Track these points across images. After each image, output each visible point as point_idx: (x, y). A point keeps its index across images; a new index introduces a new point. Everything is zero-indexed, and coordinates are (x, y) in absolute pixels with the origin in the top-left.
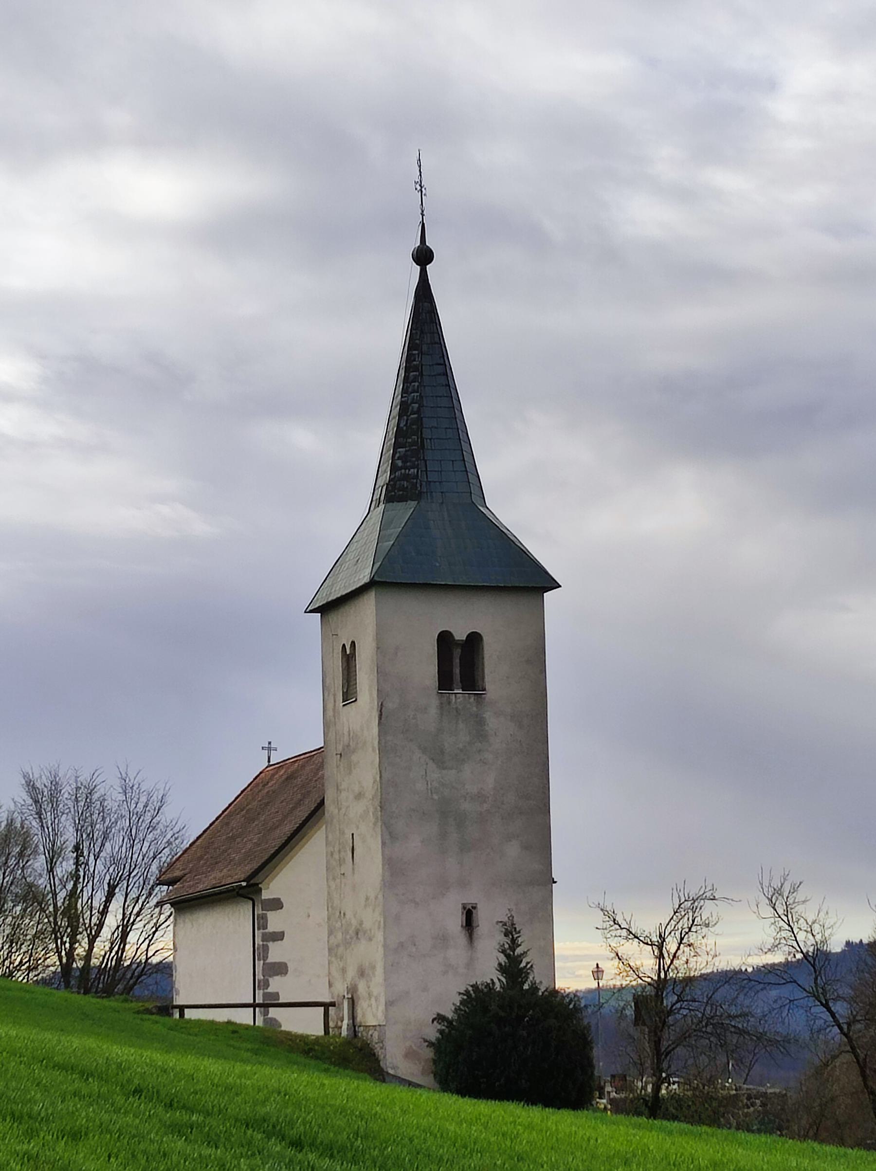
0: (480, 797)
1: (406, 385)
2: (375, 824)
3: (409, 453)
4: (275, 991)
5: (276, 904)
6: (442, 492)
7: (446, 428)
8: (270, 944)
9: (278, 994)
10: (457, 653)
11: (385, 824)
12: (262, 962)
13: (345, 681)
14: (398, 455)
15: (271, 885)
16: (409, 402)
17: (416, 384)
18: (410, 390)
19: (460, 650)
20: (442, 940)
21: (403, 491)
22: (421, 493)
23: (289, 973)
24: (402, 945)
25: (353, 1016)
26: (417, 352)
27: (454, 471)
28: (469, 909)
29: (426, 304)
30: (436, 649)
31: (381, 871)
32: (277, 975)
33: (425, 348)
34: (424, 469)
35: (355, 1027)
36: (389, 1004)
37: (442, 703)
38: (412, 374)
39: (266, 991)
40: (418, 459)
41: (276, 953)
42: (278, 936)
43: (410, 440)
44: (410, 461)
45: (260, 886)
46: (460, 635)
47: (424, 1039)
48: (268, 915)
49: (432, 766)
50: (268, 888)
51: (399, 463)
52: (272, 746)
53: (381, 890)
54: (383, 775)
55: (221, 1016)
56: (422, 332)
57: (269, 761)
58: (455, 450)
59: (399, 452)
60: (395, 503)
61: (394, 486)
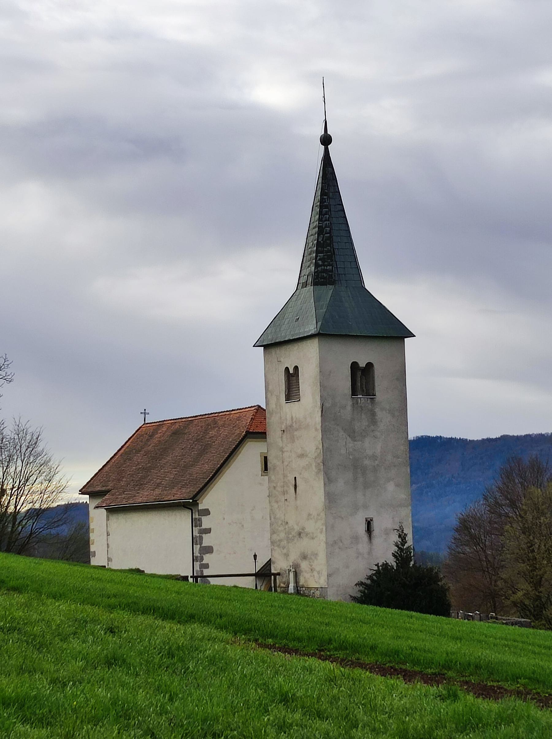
0: (374, 457)
1: (321, 216)
2: (317, 473)
3: (326, 257)
4: (207, 563)
5: (206, 512)
6: (346, 280)
7: (345, 243)
8: (204, 535)
9: (208, 564)
10: (359, 374)
11: (326, 473)
12: (199, 546)
13: (286, 388)
14: (319, 258)
15: (203, 501)
16: (324, 226)
17: (328, 216)
18: (324, 219)
19: (361, 373)
20: (355, 539)
21: (324, 279)
22: (335, 280)
23: (214, 551)
24: (335, 542)
25: (296, 582)
26: (326, 197)
27: (351, 268)
28: (369, 521)
29: (329, 169)
30: (350, 371)
31: (323, 500)
32: (207, 553)
33: (331, 194)
34: (336, 267)
35: (297, 587)
36: (329, 576)
37: (353, 404)
38: (324, 210)
39: (202, 563)
40: (332, 261)
41: (207, 540)
42: (208, 531)
43: (326, 249)
44: (327, 262)
45: (198, 502)
46: (362, 364)
47: (350, 595)
48: (202, 519)
49: (349, 439)
50: (202, 503)
51: (320, 262)
52: (146, 411)
53: (323, 510)
54: (324, 445)
55: (229, 582)
56: (329, 185)
57: (145, 421)
58: (351, 255)
59: (320, 256)
60: (319, 286)
61: (318, 276)
